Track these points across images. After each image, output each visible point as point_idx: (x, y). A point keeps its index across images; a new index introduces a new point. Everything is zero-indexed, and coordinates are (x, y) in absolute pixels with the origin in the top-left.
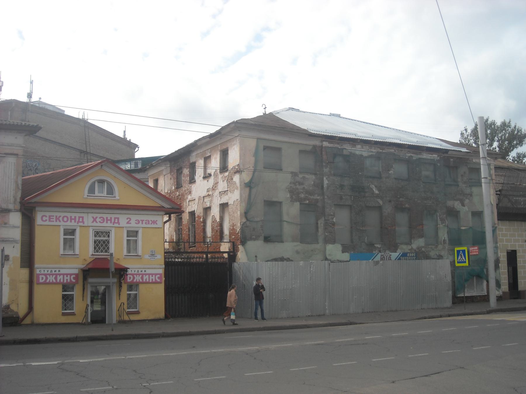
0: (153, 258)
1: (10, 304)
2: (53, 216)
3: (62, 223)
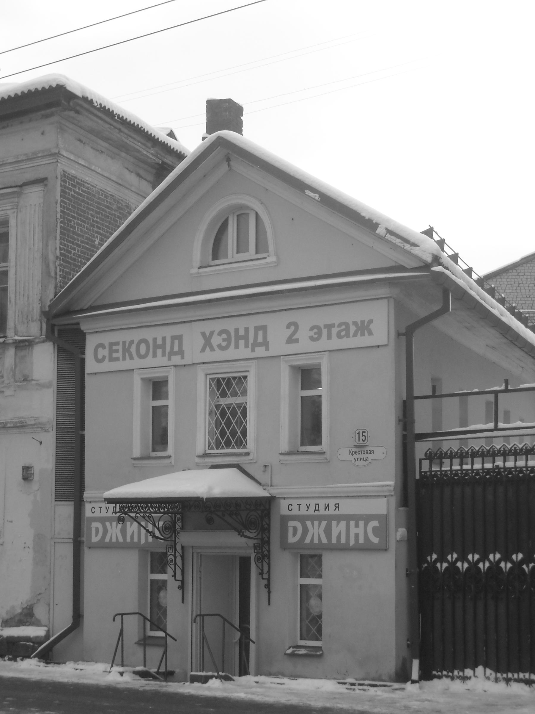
0: (361, 459)
1: (35, 603)
2: (117, 344)
3: (137, 363)
